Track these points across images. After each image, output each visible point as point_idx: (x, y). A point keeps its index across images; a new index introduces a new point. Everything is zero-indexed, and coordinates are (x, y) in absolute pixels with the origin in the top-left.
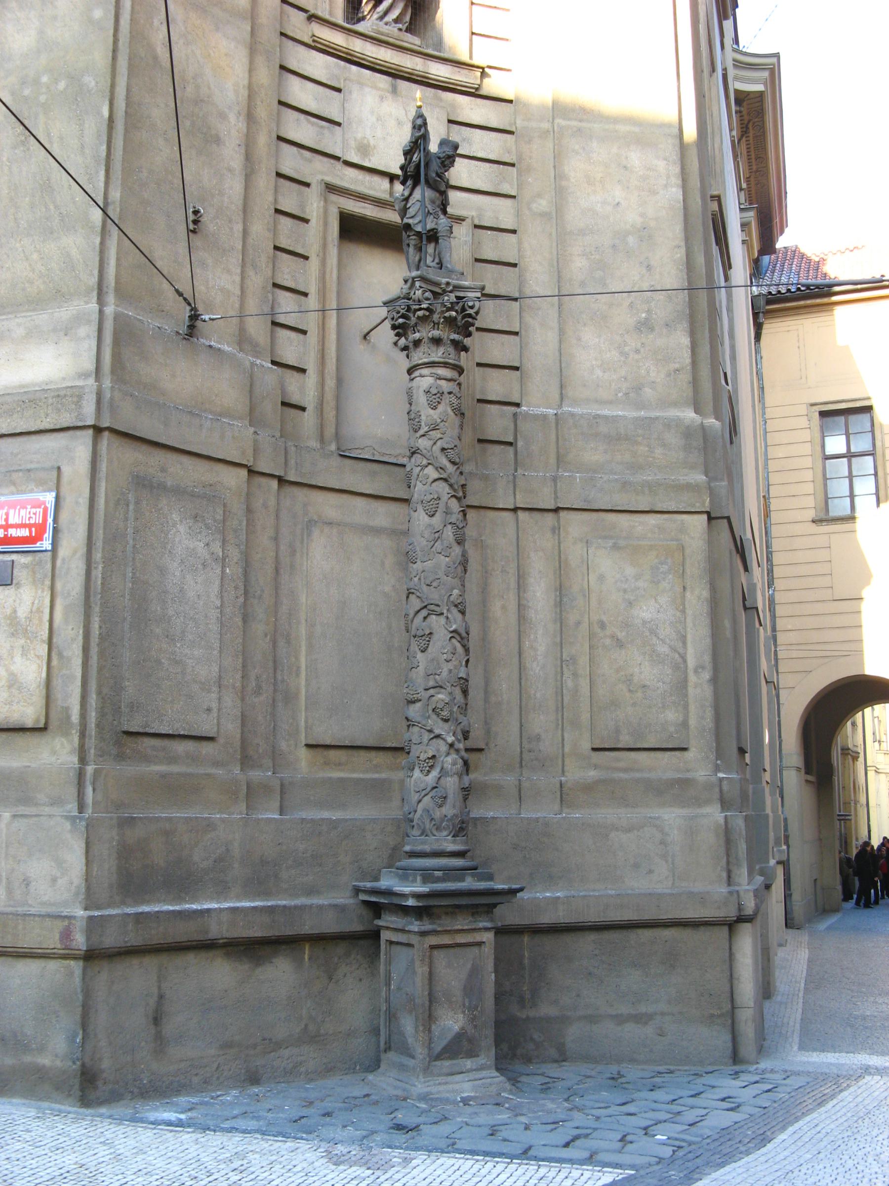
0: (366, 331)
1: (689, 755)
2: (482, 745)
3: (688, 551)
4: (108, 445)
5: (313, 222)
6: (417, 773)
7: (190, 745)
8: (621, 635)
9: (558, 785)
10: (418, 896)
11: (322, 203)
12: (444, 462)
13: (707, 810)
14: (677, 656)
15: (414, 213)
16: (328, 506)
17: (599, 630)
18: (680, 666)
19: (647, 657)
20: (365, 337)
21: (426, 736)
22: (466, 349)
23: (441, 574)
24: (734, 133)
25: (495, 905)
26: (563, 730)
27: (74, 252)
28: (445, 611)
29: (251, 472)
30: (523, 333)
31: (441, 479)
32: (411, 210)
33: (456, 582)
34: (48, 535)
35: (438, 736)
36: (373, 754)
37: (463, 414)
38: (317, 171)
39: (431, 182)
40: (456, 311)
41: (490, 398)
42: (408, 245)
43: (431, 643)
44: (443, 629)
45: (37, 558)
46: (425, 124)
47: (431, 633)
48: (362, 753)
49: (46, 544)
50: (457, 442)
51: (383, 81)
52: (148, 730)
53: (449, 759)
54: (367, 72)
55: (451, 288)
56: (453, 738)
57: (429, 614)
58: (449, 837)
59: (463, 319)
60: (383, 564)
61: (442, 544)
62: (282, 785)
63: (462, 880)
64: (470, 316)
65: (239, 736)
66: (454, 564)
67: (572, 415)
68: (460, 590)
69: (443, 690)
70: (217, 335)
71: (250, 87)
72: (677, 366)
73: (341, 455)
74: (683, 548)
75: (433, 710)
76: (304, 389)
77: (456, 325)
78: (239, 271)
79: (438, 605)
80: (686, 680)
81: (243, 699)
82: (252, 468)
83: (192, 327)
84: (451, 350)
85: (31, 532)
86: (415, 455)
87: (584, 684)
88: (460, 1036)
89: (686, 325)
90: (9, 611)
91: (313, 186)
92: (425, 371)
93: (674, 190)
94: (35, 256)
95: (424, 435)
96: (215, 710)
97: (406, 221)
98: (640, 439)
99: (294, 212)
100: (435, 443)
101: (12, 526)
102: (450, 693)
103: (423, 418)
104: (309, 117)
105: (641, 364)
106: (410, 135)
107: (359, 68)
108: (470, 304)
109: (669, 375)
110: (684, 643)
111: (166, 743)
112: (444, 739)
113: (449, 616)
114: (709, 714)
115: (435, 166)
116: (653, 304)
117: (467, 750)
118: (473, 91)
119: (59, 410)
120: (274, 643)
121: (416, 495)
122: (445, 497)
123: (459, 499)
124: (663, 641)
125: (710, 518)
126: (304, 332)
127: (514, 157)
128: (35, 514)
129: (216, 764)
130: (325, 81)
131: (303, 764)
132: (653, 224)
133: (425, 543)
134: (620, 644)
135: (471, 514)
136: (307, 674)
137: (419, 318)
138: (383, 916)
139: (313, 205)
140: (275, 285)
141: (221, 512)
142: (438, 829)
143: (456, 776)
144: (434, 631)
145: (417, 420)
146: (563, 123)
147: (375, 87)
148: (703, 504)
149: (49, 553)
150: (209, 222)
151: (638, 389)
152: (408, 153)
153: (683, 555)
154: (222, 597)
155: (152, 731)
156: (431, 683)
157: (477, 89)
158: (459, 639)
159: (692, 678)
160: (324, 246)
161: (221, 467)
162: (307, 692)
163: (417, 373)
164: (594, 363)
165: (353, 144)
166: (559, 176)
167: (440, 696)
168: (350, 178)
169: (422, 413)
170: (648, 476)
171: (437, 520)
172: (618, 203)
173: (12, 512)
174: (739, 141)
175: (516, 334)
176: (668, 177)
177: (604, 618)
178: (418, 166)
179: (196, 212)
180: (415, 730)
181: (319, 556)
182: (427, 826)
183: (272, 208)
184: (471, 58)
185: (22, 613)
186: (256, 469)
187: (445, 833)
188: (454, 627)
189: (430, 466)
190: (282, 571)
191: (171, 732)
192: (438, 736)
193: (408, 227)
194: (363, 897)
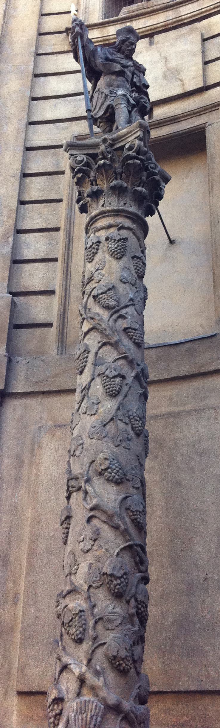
131: (15, 718)
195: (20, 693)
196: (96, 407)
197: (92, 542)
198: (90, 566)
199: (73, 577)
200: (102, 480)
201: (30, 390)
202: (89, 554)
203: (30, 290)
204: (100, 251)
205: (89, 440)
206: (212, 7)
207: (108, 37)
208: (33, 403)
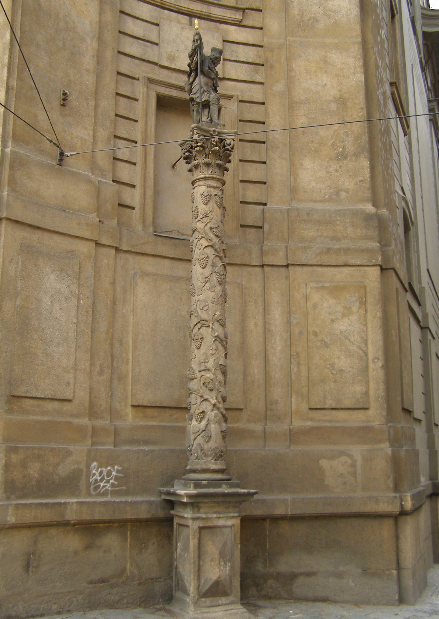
1: (371, 412)
2: (242, 406)
3: (368, 289)
4: (5, 228)
5: (140, 101)
6: (194, 422)
7: (56, 404)
8: (327, 340)
9: (288, 431)
10: (190, 496)
11: (145, 89)
12: (211, 235)
13: (382, 446)
14: (361, 352)
15: (195, 92)
16: (149, 265)
17: (313, 337)
19: (343, 353)
22: (227, 170)
23: (209, 302)
24: (422, 55)
26: (291, 397)
28: (211, 325)
29: (98, 244)
31: (209, 246)
32: (194, 89)
33: (218, 307)
35: (206, 400)
36: (174, 411)
37: (224, 208)
38: (141, 71)
39: (205, 73)
40: (219, 147)
41: (248, 201)
42: (193, 110)
43: (203, 343)
46: (200, 39)
47: (202, 338)
48: (168, 410)
50: (220, 224)
52: (28, 395)
53: (213, 413)
54: (174, 14)
55: (216, 133)
56: (215, 401)
57: (201, 327)
58: (213, 461)
59: (224, 152)
60: (181, 298)
61: (210, 284)
62: (115, 429)
63: (220, 486)
64: (228, 150)
65: (88, 399)
66: (217, 296)
67: (297, 209)
68: (221, 312)
69: (209, 372)
70: (75, 165)
71: (100, 22)
72: (361, 179)
73: (155, 235)
74: (365, 287)
75: (204, 384)
76: (133, 197)
77: (220, 155)
78: (92, 128)
79: (206, 321)
80: (367, 367)
81: (91, 379)
82: (98, 242)
83: (61, 160)
84: (217, 170)
86: (195, 232)
87: (304, 369)
88: (217, 583)
89: (366, 154)
91: (141, 79)
92: (201, 183)
93: (359, 75)
95: (200, 220)
96: (72, 384)
97: (191, 96)
99: (129, 95)
100: (206, 225)
102: (214, 374)
103: (199, 210)
104: (138, 40)
105: (339, 178)
107: (169, 12)
108: (228, 142)
109: (356, 184)
110: (366, 344)
111: (40, 402)
112: (209, 402)
113: (214, 327)
114: (382, 387)
115: (207, 64)
116: (346, 143)
117: (226, 409)
118: (239, 23)
120: (112, 344)
121: (195, 256)
122: (211, 257)
123: (221, 258)
124: (353, 343)
125: (382, 269)
126: (135, 164)
127: (263, 61)
130: (148, 20)
131: (130, 416)
132: (346, 96)
133: (200, 284)
134: (326, 346)
135: (228, 268)
136: (133, 364)
138: (175, 508)
139: (139, 90)
140: (115, 137)
141: (78, 267)
142: (206, 456)
143: (217, 424)
144: (204, 336)
145: (196, 212)
146: (292, 39)
147: (179, 22)
150: (73, 98)
151: (337, 192)
152: (191, 56)
153: (365, 291)
154: (77, 318)
155: (31, 395)
156: (202, 368)
157: (241, 22)
158: (220, 341)
159: (371, 365)
160: (146, 114)
161: (77, 241)
162: (132, 374)
163: (196, 185)
164: (311, 178)
165: (164, 55)
166: (290, 70)
167: (208, 375)
169: (199, 207)
170: (345, 244)
171: (207, 271)
172: (325, 84)
174: (426, 63)
175: (264, 163)
176: (355, 68)
177: (317, 330)
178: (197, 63)
181: (143, 293)
182: (200, 454)
183: (114, 92)
184: (237, 3)
186: (101, 243)
187: (210, 458)
188: (216, 334)
189: (203, 238)
190: (118, 303)
191: (43, 396)
192: (206, 400)
193: (192, 100)
194: (164, 497)
195: (133, 406)
196: (214, 288)
197: (215, 351)
198: (215, 361)
199: (206, 364)
200: (218, 324)
201: (129, 249)
202: (214, 356)
203: (121, 181)
204: (211, 202)
205: (211, 304)
206: (231, 19)
207: (165, 3)
208: (130, 257)
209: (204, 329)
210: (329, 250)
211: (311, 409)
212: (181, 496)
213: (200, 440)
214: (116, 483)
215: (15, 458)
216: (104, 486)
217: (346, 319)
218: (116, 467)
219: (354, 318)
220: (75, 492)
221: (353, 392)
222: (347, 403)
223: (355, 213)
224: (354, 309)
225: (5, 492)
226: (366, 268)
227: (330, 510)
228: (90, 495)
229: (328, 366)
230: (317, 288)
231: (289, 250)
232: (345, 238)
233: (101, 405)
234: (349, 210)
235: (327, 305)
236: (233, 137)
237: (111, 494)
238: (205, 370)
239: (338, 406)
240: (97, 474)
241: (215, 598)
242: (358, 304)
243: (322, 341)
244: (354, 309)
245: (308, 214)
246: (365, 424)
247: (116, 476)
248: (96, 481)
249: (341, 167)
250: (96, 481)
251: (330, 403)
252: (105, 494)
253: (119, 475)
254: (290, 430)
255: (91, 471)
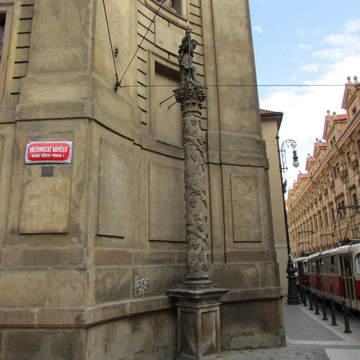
0: (161, 102)
1: (263, 243)
8: (241, 205)
10: (200, 295)
12: (198, 143)
14: (258, 212)
18: (258, 215)
20: (161, 104)
21: (195, 237)
25: (219, 297)
27: (78, 55)
30: (208, 108)
34: (70, 157)
36: (168, 244)
44: (200, 200)
45: (64, 166)
49: (69, 160)
51: (166, 22)
63: (209, 287)
67: (225, 134)
72: (253, 122)
75: (198, 228)
79: (198, 192)
80: (260, 219)
85: (62, 156)
87: (230, 220)
90: (52, 186)
91: (147, 50)
94: (61, 55)
98: (244, 143)
101: (54, 153)
102: (203, 222)
103: (191, 129)
106: (185, 35)
108: (204, 93)
109: (250, 124)
110: (259, 208)
112: (202, 238)
119: (74, 111)
121: (189, 155)
128: (64, 149)
129: (125, 247)
131: (148, 247)
132: (244, 78)
134: (241, 208)
137: (189, 96)
148: (263, 164)
149: (70, 164)
151: (242, 127)
156: (197, 218)
159: (262, 219)
168: (157, 51)
173: (54, 148)
176: (248, 65)
177: (236, 199)
179: (117, 50)
180: (191, 235)
185: (58, 187)
191: (112, 235)
195: (150, 241)
209: (197, 197)
210: (240, 157)
211: (235, 242)
212: (195, 295)
213: (197, 260)
214: (146, 288)
215: (100, 276)
216: (141, 291)
217: (250, 194)
218: (146, 278)
219: (253, 193)
220: (127, 296)
221: (253, 234)
222: (252, 239)
223: (252, 139)
224: (253, 189)
225: (96, 299)
226: (258, 168)
227: (248, 298)
228: (134, 297)
229: (242, 219)
230: (236, 177)
231: (222, 156)
232: (247, 152)
233: (136, 240)
234: (249, 137)
235: (240, 187)
236: (206, 90)
237: (144, 296)
238: (198, 220)
239: (248, 240)
240: (138, 283)
241: (209, 356)
242: (255, 186)
243: (239, 205)
244: (253, 189)
245: (230, 138)
246: (259, 250)
247: (146, 284)
248: (137, 288)
249: (243, 115)
250: (137, 287)
251: (243, 239)
252: (140, 296)
253: (148, 283)
254: (225, 253)
255: (135, 282)
